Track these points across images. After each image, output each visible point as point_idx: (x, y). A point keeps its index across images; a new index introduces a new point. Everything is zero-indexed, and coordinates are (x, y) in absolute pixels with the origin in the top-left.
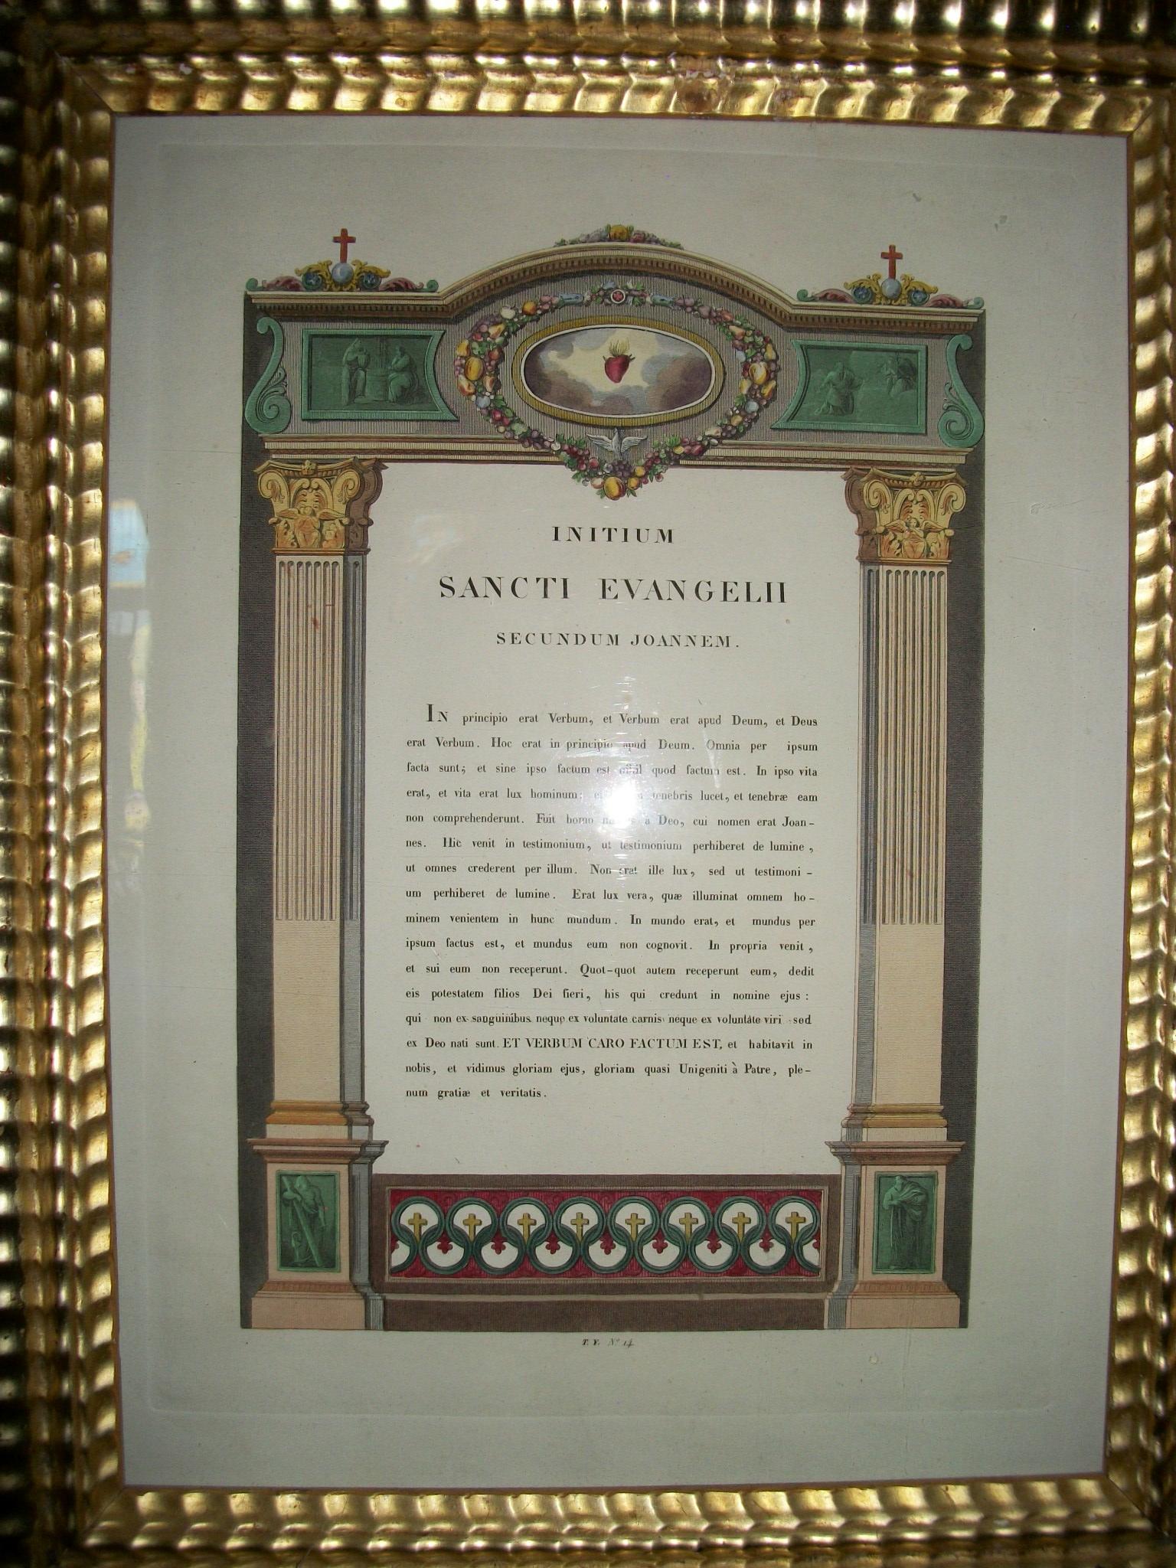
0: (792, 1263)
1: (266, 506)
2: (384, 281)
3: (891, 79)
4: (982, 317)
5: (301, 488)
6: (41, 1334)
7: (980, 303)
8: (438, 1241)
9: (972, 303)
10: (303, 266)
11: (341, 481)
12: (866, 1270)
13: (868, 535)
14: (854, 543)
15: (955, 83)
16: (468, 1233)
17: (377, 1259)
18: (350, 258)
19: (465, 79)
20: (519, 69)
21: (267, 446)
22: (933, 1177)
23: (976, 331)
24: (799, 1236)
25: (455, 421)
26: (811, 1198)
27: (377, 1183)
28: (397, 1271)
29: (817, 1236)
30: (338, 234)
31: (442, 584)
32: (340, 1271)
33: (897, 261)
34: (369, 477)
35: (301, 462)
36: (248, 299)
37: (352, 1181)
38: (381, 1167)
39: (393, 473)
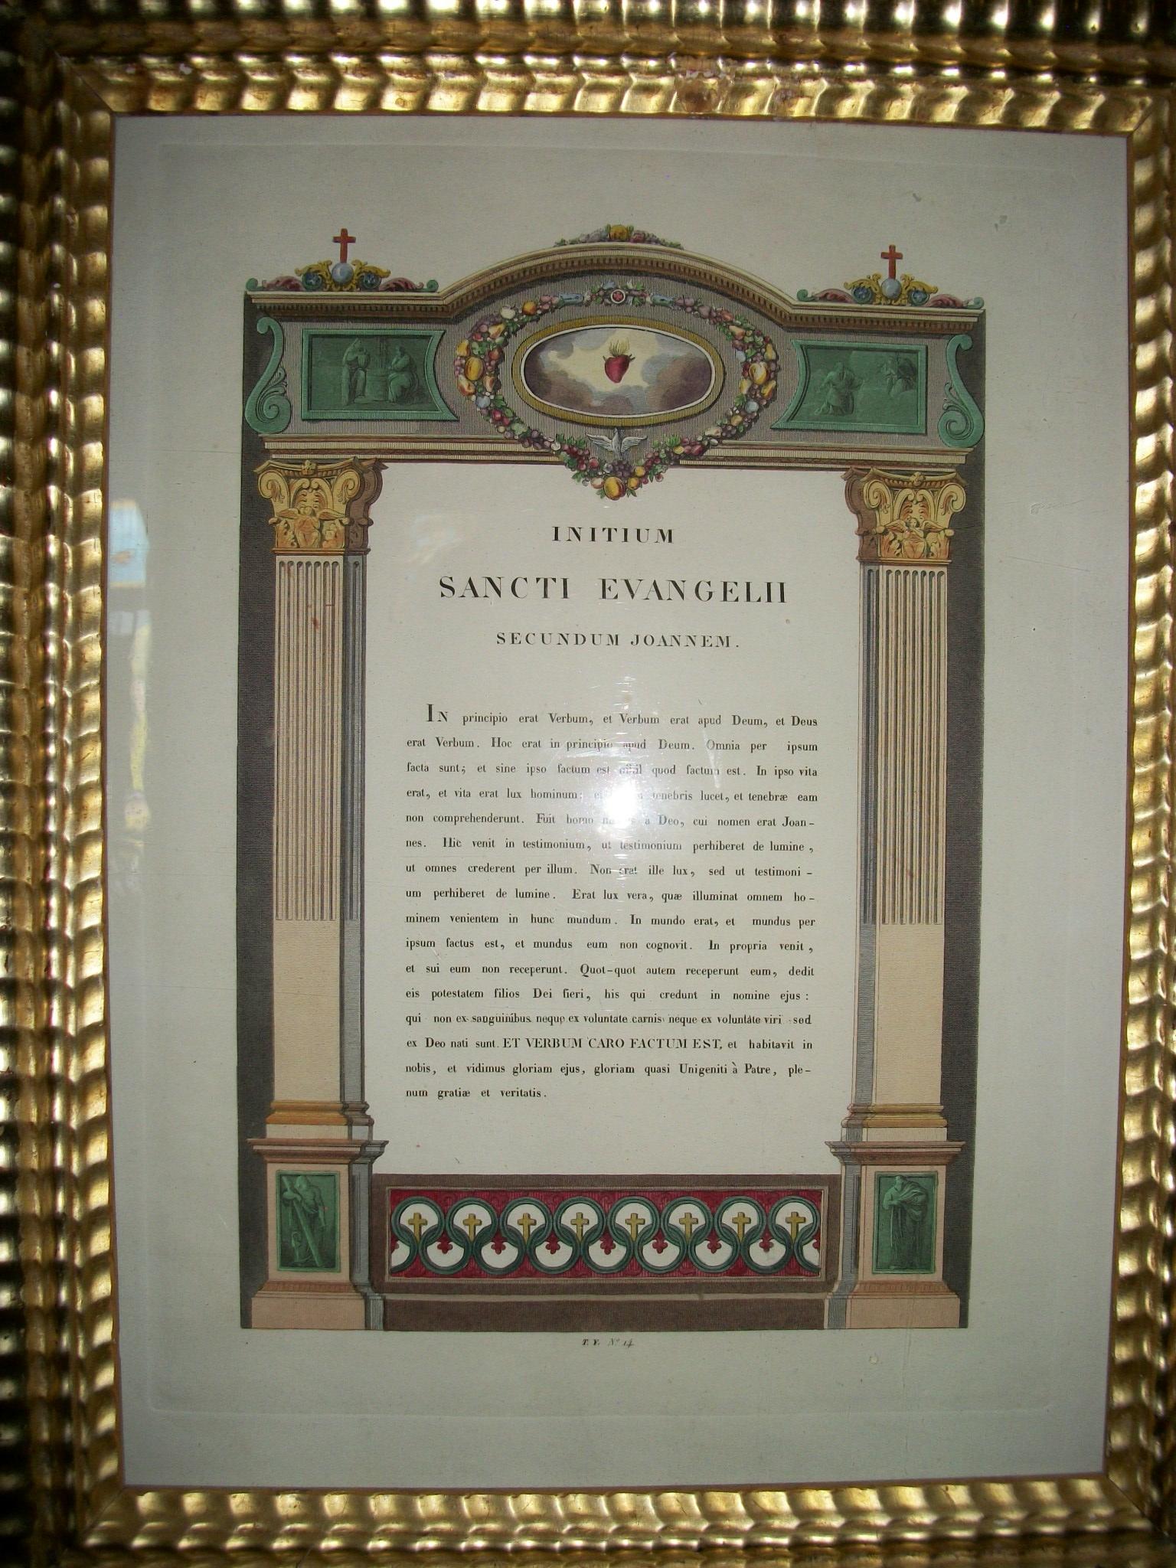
0: (792, 1263)
1: (266, 506)
2: (384, 281)
3: (891, 79)
4: (982, 317)
5: (301, 488)
6: (41, 1334)
7: (980, 303)
8: (438, 1241)
9: (972, 303)
10: (303, 266)
11: (341, 481)
12: (866, 1270)
13: (868, 535)
14: (854, 543)
15: (955, 83)
16: (468, 1233)
17: (377, 1259)
18: (350, 258)
19: (465, 79)
20: (519, 69)
21: (267, 446)
22: (933, 1177)
23: (976, 331)
24: (799, 1236)
25: (455, 421)
26: (811, 1198)
27: (377, 1183)
28: (397, 1271)
29: (817, 1236)
30: (338, 234)
32: (340, 1271)
33: (897, 261)
34: (369, 477)
35: (301, 462)
36: (248, 299)
37: (352, 1181)
38: (381, 1167)
39: (393, 473)
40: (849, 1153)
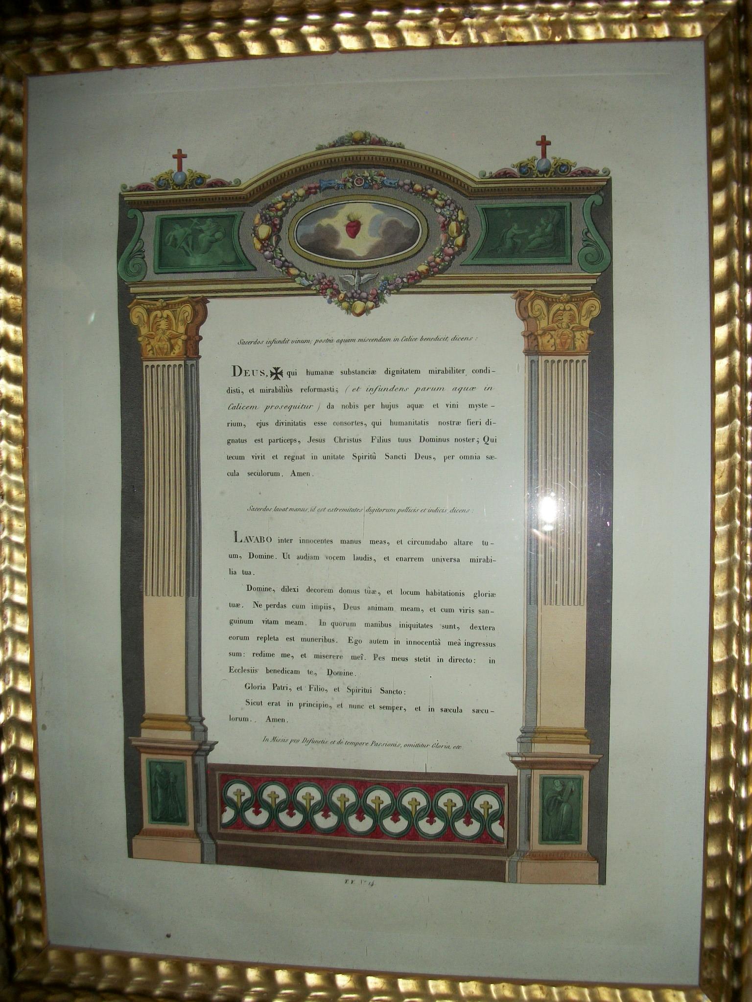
0: (485, 835)
1: (136, 330)
2: (208, 180)
4: (609, 181)
5: (559, 310)
7: (607, 172)
8: (427, 817)
9: (233, 183)
10: (516, 162)
11: (587, 305)
12: (536, 845)
13: (531, 336)
14: (521, 344)
16: (305, 804)
17: (212, 819)
18: (184, 170)
21: (132, 290)
22: (580, 780)
23: (605, 189)
24: (489, 817)
25: (252, 270)
26: (497, 792)
27: (211, 769)
28: (225, 826)
29: (502, 819)
30: (176, 153)
31: (354, 456)
32: (581, 844)
33: (183, 159)
34: (199, 307)
35: (157, 300)
36: (121, 197)
37: (195, 767)
38: (214, 758)
39: (213, 305)
40: (526, 764)
